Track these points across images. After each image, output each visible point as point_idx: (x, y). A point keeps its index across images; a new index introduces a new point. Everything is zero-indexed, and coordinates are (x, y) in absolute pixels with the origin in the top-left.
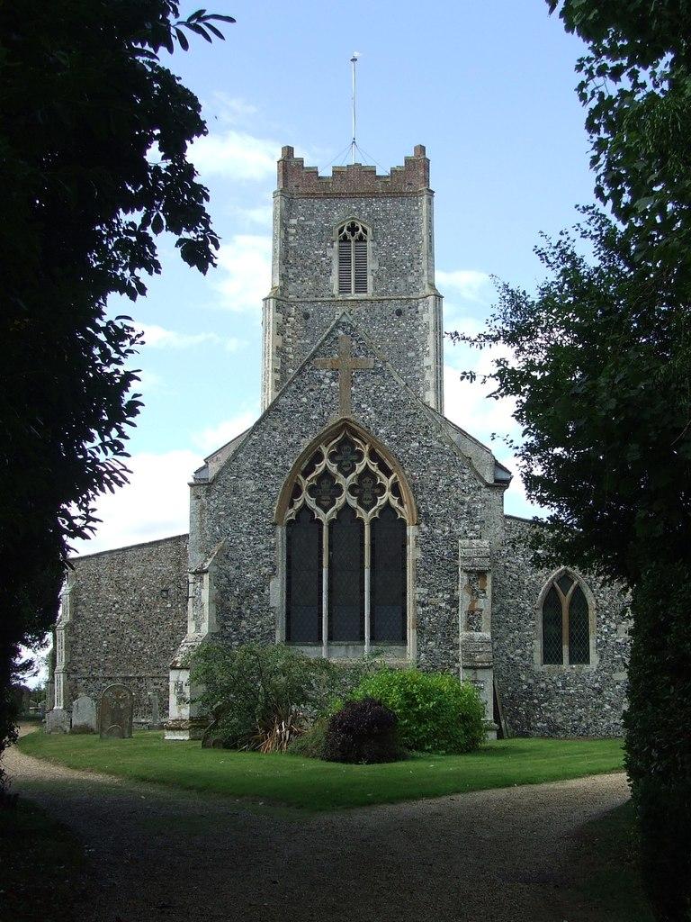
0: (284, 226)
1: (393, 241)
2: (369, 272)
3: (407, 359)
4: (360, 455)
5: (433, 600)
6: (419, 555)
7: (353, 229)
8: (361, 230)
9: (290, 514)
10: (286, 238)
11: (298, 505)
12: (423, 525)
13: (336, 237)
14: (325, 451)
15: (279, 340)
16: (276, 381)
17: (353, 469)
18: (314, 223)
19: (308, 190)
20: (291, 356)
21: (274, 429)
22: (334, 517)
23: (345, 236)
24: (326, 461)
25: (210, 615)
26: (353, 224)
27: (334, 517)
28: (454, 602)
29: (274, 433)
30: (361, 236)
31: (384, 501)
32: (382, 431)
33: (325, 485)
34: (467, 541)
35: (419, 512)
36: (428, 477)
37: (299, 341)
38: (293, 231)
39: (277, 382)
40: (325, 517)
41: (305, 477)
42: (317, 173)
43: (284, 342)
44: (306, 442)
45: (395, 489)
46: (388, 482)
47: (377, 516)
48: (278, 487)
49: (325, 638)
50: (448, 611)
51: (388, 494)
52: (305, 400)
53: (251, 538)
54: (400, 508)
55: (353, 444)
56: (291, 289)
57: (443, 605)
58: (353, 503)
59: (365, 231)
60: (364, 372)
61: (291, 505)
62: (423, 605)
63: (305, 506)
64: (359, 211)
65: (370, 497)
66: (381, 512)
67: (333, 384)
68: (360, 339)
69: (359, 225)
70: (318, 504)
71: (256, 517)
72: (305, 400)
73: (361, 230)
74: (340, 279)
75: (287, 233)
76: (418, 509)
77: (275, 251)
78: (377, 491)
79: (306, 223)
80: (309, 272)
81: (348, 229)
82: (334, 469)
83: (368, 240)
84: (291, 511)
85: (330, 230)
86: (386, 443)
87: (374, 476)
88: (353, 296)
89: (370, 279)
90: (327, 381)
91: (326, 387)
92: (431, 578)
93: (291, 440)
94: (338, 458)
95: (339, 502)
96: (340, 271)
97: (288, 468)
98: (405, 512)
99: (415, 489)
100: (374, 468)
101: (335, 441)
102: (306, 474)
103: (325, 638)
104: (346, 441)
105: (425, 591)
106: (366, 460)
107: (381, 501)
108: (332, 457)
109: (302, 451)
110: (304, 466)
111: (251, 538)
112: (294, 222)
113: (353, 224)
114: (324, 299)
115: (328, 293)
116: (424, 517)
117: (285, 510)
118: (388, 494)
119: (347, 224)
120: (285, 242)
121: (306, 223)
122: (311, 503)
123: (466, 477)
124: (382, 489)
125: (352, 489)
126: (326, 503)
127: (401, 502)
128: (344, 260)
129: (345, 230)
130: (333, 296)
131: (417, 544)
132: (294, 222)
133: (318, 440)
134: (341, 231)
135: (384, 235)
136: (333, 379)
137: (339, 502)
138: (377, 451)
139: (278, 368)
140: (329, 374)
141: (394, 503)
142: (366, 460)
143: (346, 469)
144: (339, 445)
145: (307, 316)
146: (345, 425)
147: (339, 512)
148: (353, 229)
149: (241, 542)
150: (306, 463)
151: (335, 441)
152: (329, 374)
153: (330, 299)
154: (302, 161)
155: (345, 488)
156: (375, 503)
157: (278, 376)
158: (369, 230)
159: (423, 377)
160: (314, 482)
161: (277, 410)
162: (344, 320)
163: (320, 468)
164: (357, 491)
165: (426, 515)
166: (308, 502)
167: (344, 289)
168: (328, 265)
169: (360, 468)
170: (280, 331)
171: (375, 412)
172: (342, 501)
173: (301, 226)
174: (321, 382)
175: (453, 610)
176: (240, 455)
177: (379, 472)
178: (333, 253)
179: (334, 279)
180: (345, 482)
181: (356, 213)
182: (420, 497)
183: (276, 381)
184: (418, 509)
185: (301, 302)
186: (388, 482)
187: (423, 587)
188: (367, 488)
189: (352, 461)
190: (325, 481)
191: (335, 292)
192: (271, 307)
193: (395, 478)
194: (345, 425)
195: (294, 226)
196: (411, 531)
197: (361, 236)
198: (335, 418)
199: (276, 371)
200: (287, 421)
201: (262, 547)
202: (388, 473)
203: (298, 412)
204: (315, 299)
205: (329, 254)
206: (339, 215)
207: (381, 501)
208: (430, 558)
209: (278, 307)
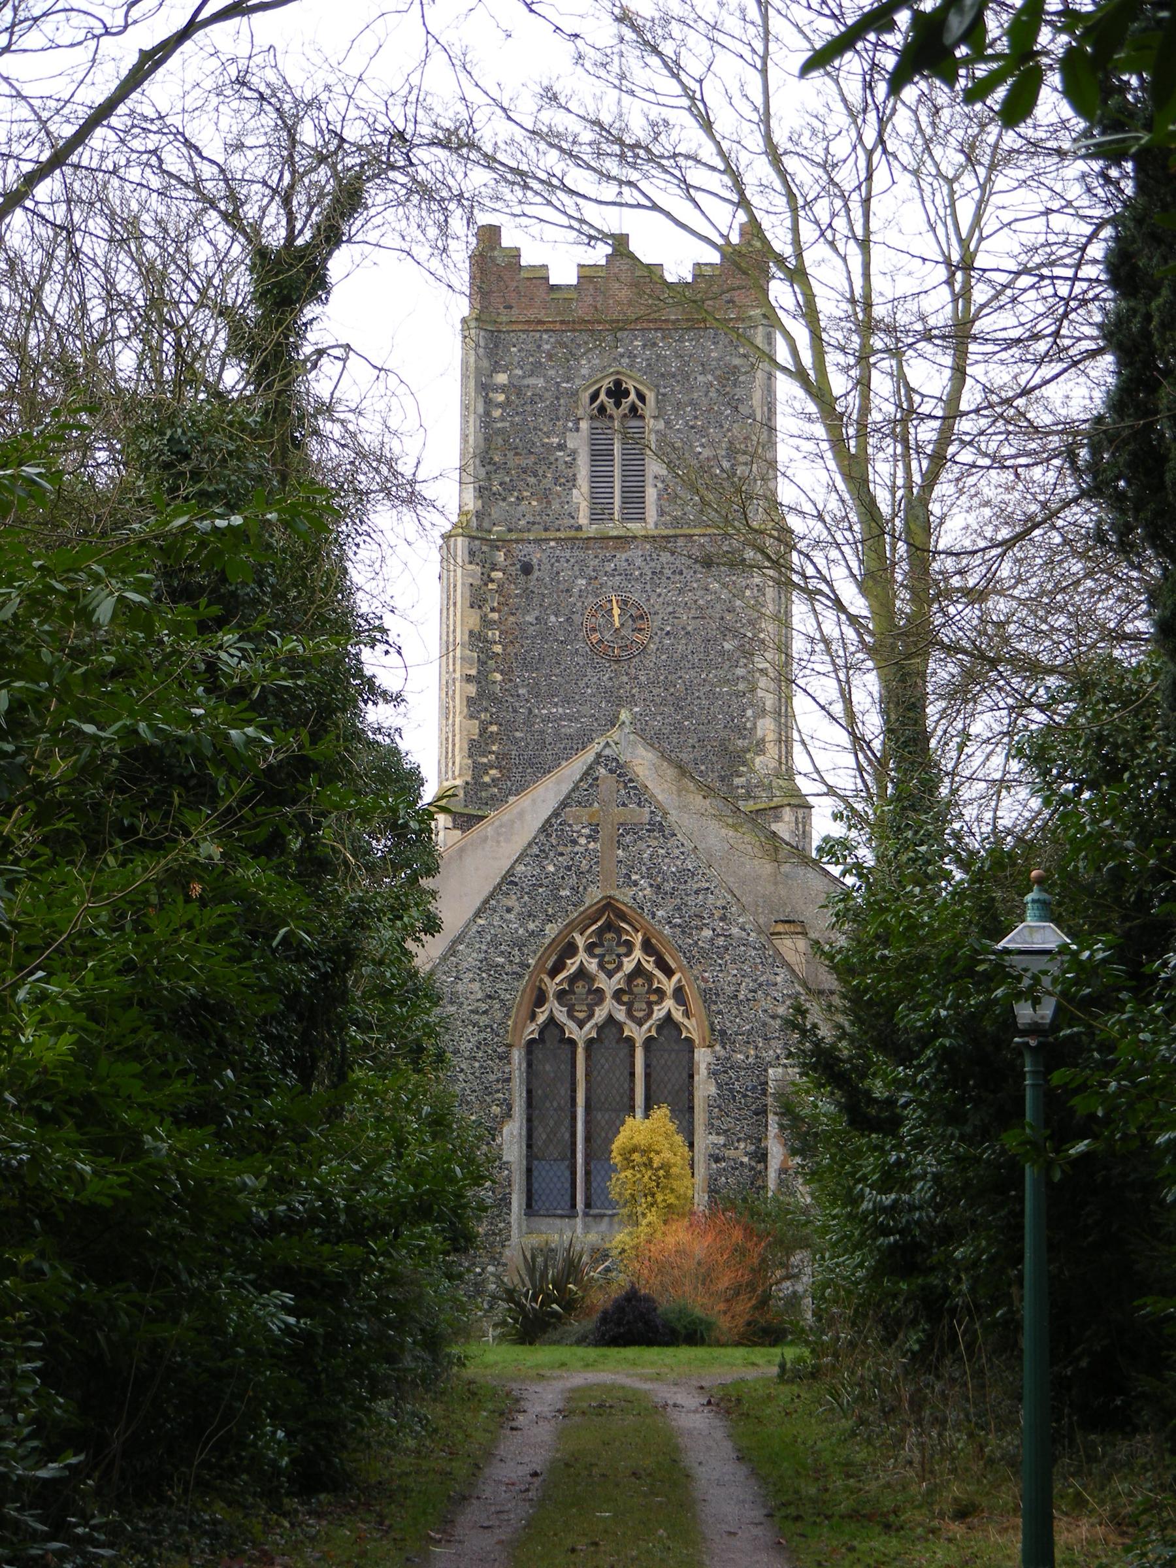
0: (485, 388)
1: (696, 418)
2: (649, 480)
3: (722, 653)
4: (629, 946)
5: (731, 1153)
6: (713, 1090)
7: (618, 393)
8: (633, 396)
9: (531, 1031)
10: (487, 413)
11: (541, 1018)
12: (718, 1048)
13: (584, 407)
14: (580, 941)
15: (474, 620)
16: (469, 699)
17: (620, 967)
18: (541, 382)
19: (531, 314)
20: (498, 649)
21: (509, 910)
22: (594, 1034)
23: (602, 409)
24: (582, 956)
25: (520, 1205)
26: (618, 383)
27: (594, 1034)
28: (762, 1156)
29: (508, 916)
30: (633, 408)
31: (662, 1014)
32: (660, 913)
33: (580, 988)
34: (780, 1070)
35: (713, 1030)
36: (726, 980)
37: (512, 619)
38: (501, 398)
39: (470, 701)
40: (638, 1034)
41: (553, 978)
42: (547, 279)
43: (486, 622)
44: (552, 930)
45: (679, 995)
46: (669, 986)
47: (653, 1033)
48: (517, 993)
49: (580, 1205)
50: (752, 1168)
51: (669, 1003)
52: (551, 868)
53: (477, 1064)
54: (686, 1022)
55: (619, 931)
56: (495, 512)
57: (745, 1160)
58: (621, 1015)
59: (642, 397)
60: (630, 828)
61: (533, 1017)
62: (717, 1160)
63: (551, 1020)
64: (633, 360)
65: (644, 1006)
66: (659, 1028)
67: (592, 846)
68: (631, 781)
69: (630, 385)
70: (570, 1015)
71: (483, 1035)
72: (551, 868)
73: (633, 396)
74: (593, 496)
75: (488, 402)
76: (712, 1024)
77: (465, 438)
78: (654, 998)
79: (526, 382)
80: (532, 480)
81: (609, 393)
82: (592, 966)
83: (647, 414)
84: (533, 1027)
85: (574, 394)
86: (667, 930)
87: (649, 977)
88: (613, 529)
89: (651, 494)
90: (583, 841)
91: (582, 849)
92: (728, 1123)
93: (531, 926)
94: (598, 951)
95: (600, 1014)
96: (594, 477)
97: (528, 966)
98: (692, 1028)
99: (708, 996)
100: (650, 966)
101: (594, 927)
102: (553, 973)
103: (580, 1205)
104: (609, 927)
105: (721, 1140)
106: (638, 953)
107: (659, 1013)
108: (590, 948)
109: (547, 941)
110: (549, 964)
111: (477, 1064)
112: (502, 378)
113: (618, 383)
114: (558, 535)
115: (568, 522)
116: (719, 1036)
117: (524, 1026)
118: (669, 1003)
119: (607, 383)
120: (486, 420)
121: (526, 382)
122: (561, 1016)
123: (779, 979)
124: (660, 993)
125: (618, 995)
126: (581, 1015)
127: (687, 1014)
128: (601, 455)
129: (603, 396)
130: (579, 528)
131: (713, 1074)
132: (502, 378)
133: (570, 927)
134: (594, 397)
135: (679, 406)
136: (591, 838)
137: (600, 1014)
138: (654, 941)
139: (473, 672)
140: (586, 831)
141: (678, 1015)
142: (638, 953)
143: (610, 967)
144: (600, 932)
145: (527, 569)
146: (609, 904)
147: (600, 1028)
148: (618, 393)
149: (462, 1070)
150: (554, 958)
151: (594, 927)
152: (586, 831)
153: (573, 533)
154: (516, 253)
155: (609, 994)
156: (650, 1014)
157: (472, 690)
158: (650, 396)
159: (753, 690)
160: (565, 986)
161: (512, 882)
162: (607, 752)
163: (572, 965)
164: (625, 998)
165: (723, 1033)
166: (557, 1014)
167: (600, 512)
168: (569, 465)
169: (629, 965)
170: (477, 601)
171: (651, 886)
172: (604, 1013)
173: (513, 388)
174: (574, 842)
175: (760, 1167)
176: (461, 947)
177: (657, 972)
178: (579, 441)
179: (580, 497)
180: (608, 985)
181: (625, 361)
182: (714, 1008)
183: (469, 699)
184: (712, 1024)
185: (517, 541)
186: (669, 986)
187: (718, 1134)
188: (637, 991)
189: (619, 956)
190: (580, 983)
191: (583, 520)
192: (459, 553)
193: (680, 980)
194: (609, 905)
195: (503, 389)
196: (703, 1057)
197: (633, 408)
198: (594, 895)
199: (469, 679)
200: (526, 898)
201: (492, 1077)
202: (669, 973)
203: (541, 886)
204: (544, 535)
205: (570, 445)
206: (591, 370)
207: (659, 1013)
208: (726, 1092)
209: (472, 553)
